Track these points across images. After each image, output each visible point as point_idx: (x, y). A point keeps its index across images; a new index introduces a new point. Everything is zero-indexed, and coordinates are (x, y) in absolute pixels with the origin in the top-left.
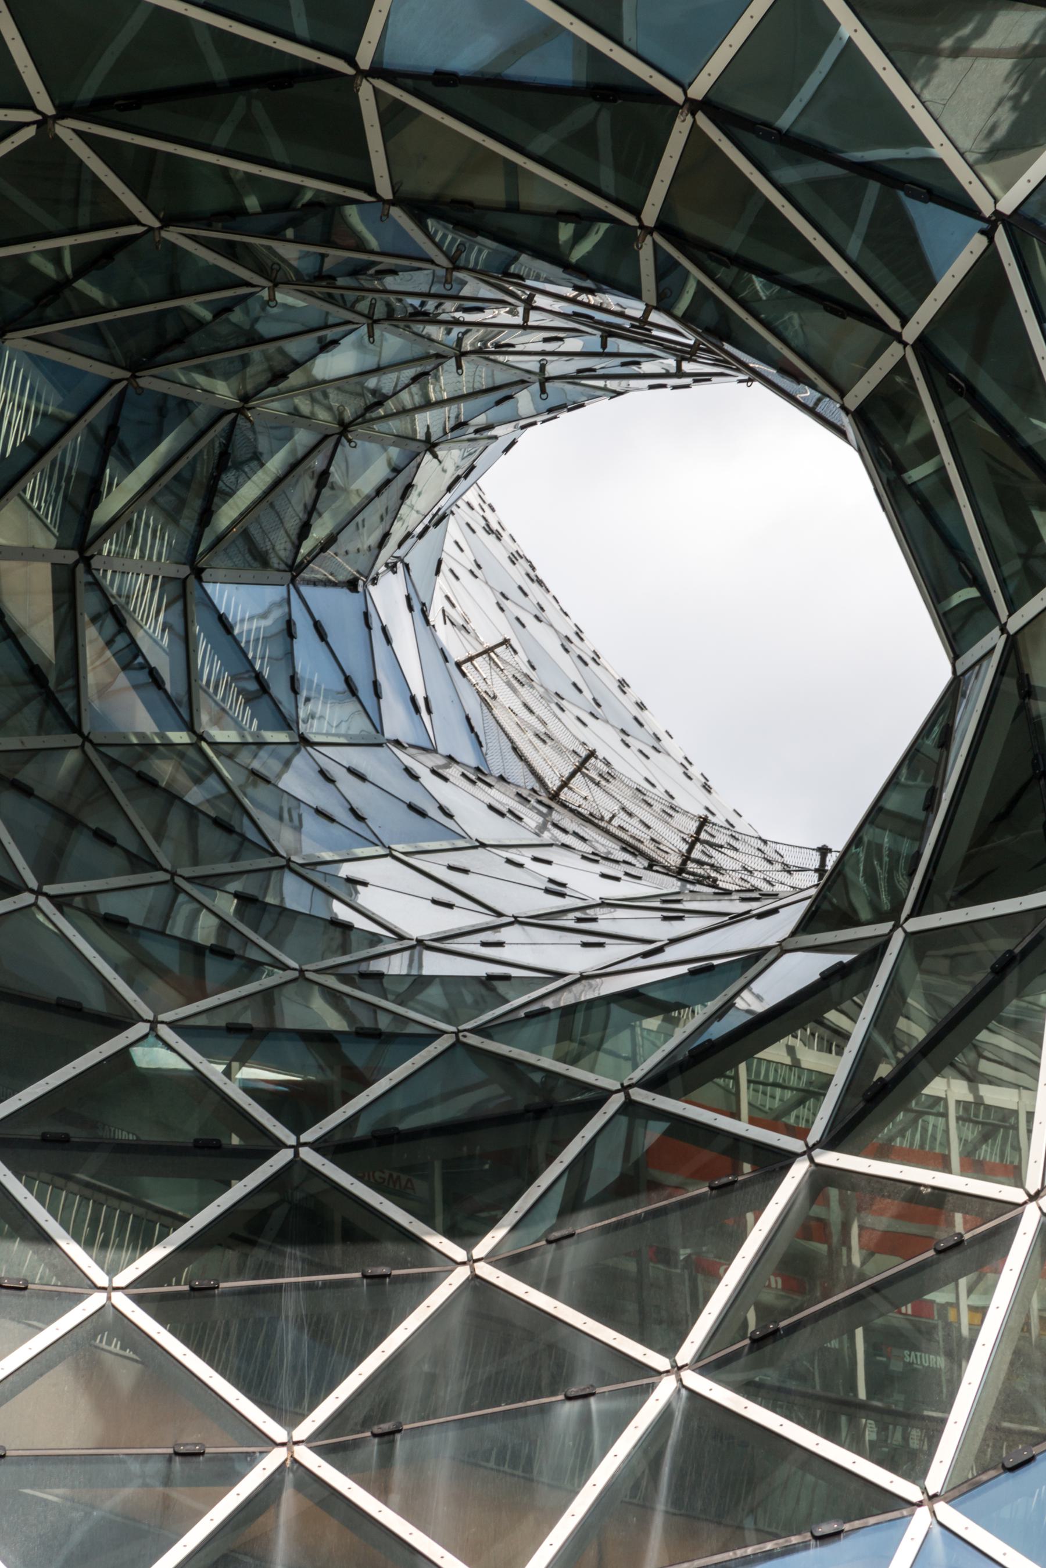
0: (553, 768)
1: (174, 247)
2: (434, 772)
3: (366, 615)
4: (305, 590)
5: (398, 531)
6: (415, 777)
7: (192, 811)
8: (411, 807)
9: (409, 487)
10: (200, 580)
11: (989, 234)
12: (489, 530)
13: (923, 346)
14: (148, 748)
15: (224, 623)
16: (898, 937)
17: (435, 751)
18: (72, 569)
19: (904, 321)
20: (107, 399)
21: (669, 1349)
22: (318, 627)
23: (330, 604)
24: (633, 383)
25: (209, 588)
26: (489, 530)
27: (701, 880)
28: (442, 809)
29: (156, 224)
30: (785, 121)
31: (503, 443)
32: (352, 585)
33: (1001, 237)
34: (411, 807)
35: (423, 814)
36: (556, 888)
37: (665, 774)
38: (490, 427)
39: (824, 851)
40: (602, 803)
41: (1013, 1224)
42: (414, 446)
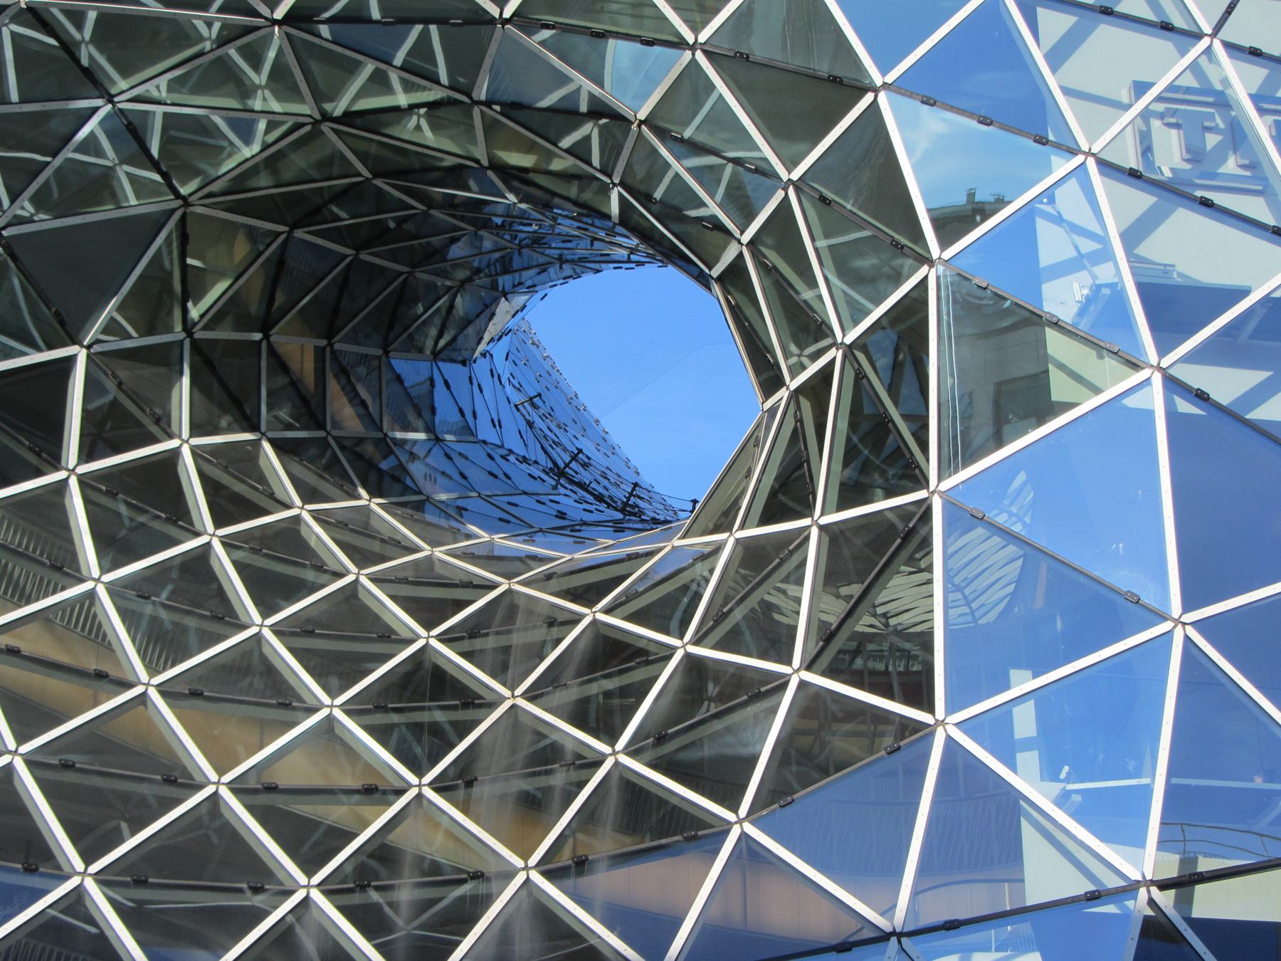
0: (562, 458)
1: (379, 190)
2: (502, 457)
3: (470, 378)
4: (441, 364)
5: (487, 337)
6: (492, 459)
7: (380, 470)
8: (490, 473)
9: (493, 314)
10: (387, 356)
11: (785, 189)
12: (533, 344)
13: (752, 244)
14: (361, 440)
15: (399, 379)
16: (731, 542)
17: (502, 447)
18: (324, 349)
19: (742, 233)
20: (343, 265)
21: (612, 743)
22: (446, 383)
23: (452, 371)
24: (603, 265)
25: (393, 361)
26: (533, 344)
27: (631, 514)
28: (506, 475)
29: (370, 176)
30: (687, 134)
31: (541, 294)
32: (464, 363)
33: (791, 191)
34: (490, 473)
35: (496, 477)
36: (561, 515)
37: (618, 467)
38: (534, 286)
39: (695, 502)
40: (585, 476)
41: (787, 683)
42: (496, 294)
